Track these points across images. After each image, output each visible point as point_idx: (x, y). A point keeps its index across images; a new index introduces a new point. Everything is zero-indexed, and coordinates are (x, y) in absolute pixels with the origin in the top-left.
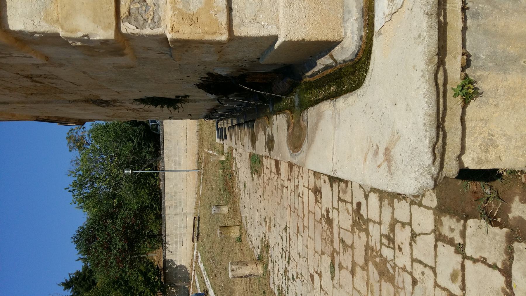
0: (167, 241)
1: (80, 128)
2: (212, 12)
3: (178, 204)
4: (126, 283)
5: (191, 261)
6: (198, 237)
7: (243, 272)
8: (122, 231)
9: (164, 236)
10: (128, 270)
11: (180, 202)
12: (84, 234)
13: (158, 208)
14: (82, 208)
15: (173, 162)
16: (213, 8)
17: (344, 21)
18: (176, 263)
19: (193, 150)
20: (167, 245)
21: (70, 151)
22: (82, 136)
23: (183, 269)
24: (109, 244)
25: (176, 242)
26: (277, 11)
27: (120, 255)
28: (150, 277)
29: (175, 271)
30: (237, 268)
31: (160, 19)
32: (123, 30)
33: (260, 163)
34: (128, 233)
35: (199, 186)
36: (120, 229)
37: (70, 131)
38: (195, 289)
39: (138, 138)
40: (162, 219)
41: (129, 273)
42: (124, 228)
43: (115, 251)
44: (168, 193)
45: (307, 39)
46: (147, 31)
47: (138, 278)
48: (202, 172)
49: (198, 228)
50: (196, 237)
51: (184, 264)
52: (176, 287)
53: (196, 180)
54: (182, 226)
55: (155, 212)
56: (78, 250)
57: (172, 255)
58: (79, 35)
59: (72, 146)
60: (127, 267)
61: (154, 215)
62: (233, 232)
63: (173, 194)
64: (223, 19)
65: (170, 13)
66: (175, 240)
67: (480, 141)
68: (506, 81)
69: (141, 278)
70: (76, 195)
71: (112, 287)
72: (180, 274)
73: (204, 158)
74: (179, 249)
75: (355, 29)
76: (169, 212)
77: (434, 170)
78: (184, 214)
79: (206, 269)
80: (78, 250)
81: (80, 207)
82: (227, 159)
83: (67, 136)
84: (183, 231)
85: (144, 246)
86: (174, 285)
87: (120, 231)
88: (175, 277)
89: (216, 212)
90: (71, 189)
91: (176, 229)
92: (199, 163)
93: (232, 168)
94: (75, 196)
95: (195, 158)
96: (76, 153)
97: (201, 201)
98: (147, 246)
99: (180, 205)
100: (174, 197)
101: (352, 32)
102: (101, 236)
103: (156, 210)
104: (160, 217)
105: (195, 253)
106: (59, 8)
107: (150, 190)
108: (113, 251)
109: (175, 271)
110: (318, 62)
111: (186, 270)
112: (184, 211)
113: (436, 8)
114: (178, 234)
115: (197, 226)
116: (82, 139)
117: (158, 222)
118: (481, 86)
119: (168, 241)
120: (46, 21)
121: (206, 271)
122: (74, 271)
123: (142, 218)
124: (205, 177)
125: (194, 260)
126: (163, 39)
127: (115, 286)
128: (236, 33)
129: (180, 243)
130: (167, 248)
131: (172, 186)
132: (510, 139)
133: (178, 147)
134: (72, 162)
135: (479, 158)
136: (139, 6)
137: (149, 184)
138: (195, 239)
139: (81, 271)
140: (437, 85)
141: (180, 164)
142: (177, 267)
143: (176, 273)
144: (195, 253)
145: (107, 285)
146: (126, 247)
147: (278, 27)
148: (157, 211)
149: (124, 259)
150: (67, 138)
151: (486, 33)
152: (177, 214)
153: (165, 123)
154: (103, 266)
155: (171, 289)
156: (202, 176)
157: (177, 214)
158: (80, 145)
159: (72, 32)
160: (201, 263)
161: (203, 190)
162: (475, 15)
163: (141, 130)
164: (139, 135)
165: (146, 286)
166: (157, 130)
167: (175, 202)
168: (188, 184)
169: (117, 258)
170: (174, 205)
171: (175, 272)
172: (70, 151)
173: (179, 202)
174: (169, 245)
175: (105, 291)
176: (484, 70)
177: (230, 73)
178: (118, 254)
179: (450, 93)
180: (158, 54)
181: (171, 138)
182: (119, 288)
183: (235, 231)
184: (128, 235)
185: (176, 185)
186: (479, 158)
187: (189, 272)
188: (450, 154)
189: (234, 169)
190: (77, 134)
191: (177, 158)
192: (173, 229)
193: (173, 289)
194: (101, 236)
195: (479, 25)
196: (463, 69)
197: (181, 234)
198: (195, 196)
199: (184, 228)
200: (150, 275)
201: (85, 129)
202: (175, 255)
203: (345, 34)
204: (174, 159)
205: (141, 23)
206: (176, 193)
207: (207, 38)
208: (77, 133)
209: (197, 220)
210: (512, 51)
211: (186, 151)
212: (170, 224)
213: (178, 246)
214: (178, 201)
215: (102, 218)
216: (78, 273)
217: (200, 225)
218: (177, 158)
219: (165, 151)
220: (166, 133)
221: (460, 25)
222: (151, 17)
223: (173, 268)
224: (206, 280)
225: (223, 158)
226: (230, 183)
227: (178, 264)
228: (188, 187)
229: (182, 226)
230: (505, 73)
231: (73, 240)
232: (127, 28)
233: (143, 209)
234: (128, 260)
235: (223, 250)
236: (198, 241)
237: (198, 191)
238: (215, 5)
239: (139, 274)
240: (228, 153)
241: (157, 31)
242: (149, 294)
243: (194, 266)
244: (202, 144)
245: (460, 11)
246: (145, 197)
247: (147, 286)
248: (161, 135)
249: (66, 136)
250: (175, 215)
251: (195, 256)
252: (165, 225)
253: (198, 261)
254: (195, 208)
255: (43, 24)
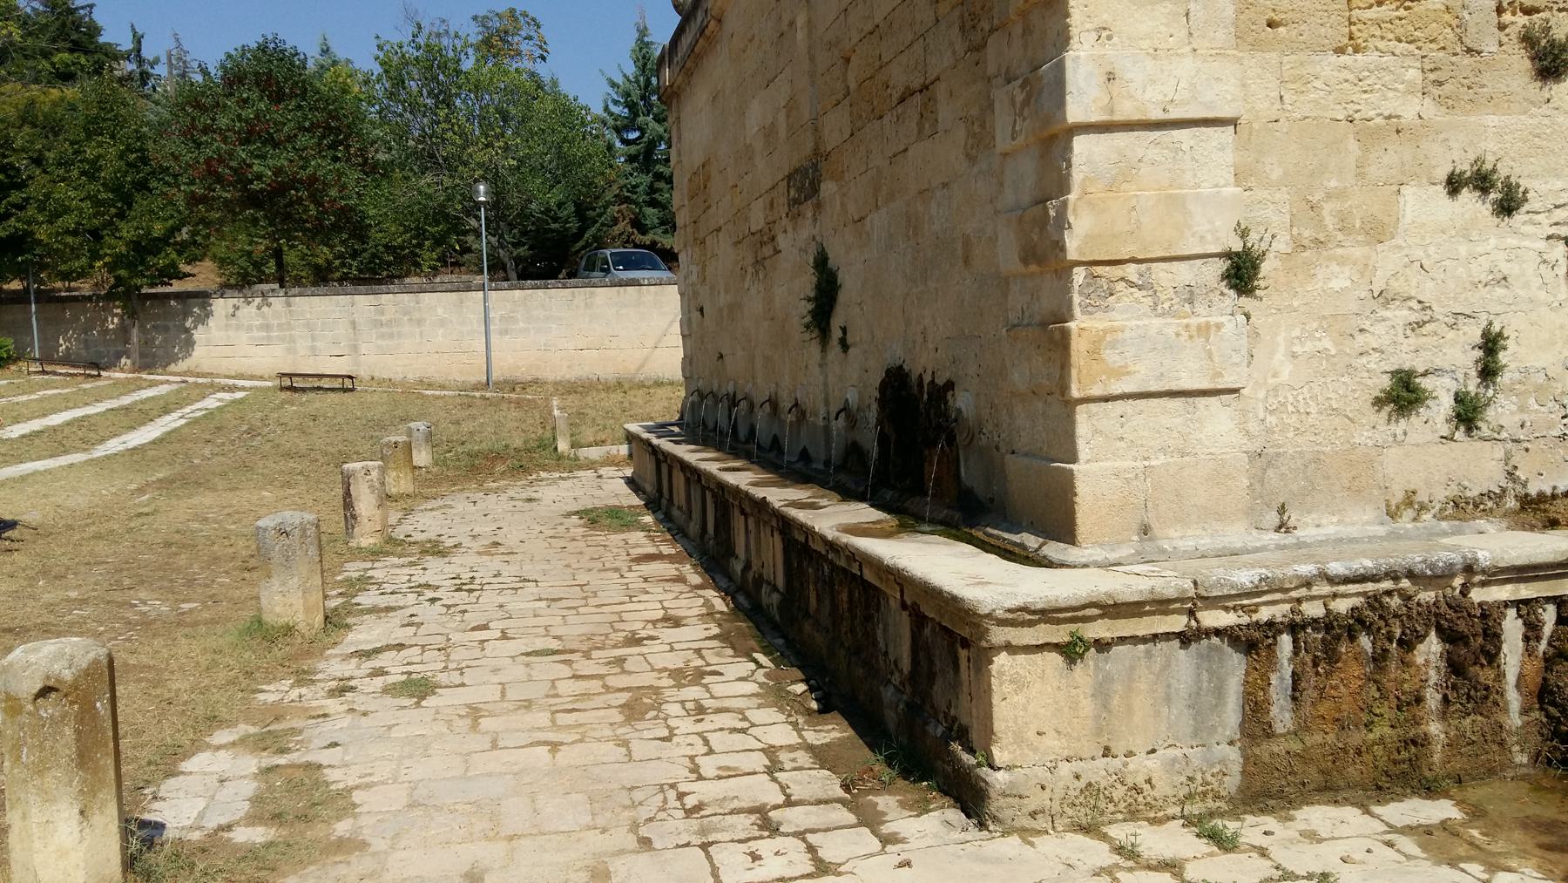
0: (271, 300)
1: (541, 47)
2: (1104, 377)
3: (384, 330)
4: (142, 186)
5: (209, 371)
6: (291, 389)
7: (362, 497)
8: (303, 175)
9: (286, 293)
10: (184, 191)
11: (391, 336)
12: (289, 69)
13: (348, 273)
14: (323, 51)
15: (512, 315)
16: (1109, 378)
17: (1101, 545)
18: (200, 327)
19: (546, 367)
20: (258, 300)
21: (475, 18)
22: (519, 53)
23: (180, 349)
24: (260, 137)
25: (267, 327)
26: (1107, 459)
27: (231, 168)
28: (163, 254)
29: (175, 326)
30: (372, 480)
31: (1091, 313)
32: (1076, 270)
33: (625, 528)
34: (297, 190)
35: (443, 387)
36: (310, 171)
37: (534, 20)
38: (133, 387)
39: (542, 213)
40: (315, 284)
41: (174, 194)
42: (313, 179)
43: (244, 156)
44: (417, 303)
45: (1077, 499)
46: (1077, 299)
47: (158, 219)
48: (488, 395)
49: (319, 388)
50: (291, 384)
51: (199, 352)
52: (124, 330)
53: (460, 378)
54: (318, 344)
55: (337, 262)
56: (236, 49)
57: (226, 316)
58: (1071, 219)
59: (490, 24)
60: (193, 188)
61: (327, 260)
62: (399, 477)
63: (417, 316)
64: (1097, 391)
65: (1100, 325)
66: (276, 322)
67: (1022, 672)
68: (1085, 698)
69: (158, 229)
70: (404, 50)
71: (129, 145)
72: (165, 340)
73: (530, 397)
74: (244, 336)
75: (1095, 558)
76: (362, 305)
77: (1000, 613)
78: (355, 348)
79: (211, 413)
80: (236, 49)
81: (325, 48)
82: (560, 458)
83: (518, 12)
84: (302, 346)
85: (257, 235)
86: (128, 322)
87: (304, 168)
88: (154, 326)
89: (415, 434)
90: (421, 40)
91: (309, 326)
92: (512, 385)
93: (544, 470)
94: (401, 47)
95: (523, 374)
96: (474, 34)
97: (402, 392)
98: (257, 243)
99: (382, 336)
100: (406, 318)
101: (1091, 555)
102: (285, 116)
103: (343, 265)
104: (322, 278)
105: (240, 383)
106: (1099, 195)
107: (403, 248)
108: (243, 150)
109: (175, 326)
110: (1024, 534)
111: (175, 359)
112: (363, 348)
113: (1158, 597)
114: (293, 332)
115: (326, 383)
116: (512, 53)
117: (303, 274)
118: (1079, 666)
119: (269, 305)
120: (1084, 179)
121: (204, 416)
122: (99, 17)
123: (336, 228)
124: (478, 402)
125: (217, 380)
126: (1065, 315)
127: (132, 153)
128: (1079, 408)
129: (263, 338)
130: (249, 303)
131: (440, 311)
132: (1025, 709)
133: (554, 326)
134: (444, 21)
135: (1003, 674)
136: (1105, 288)
137: (420, 246)
138: (286, 382)
139: (101, 40)
140: (1084, 607)
141: (505, 332)
142: (187, 331)
143: (167, 329)
144: (240, 383)
145: (136, 131)
146: (256, 186)
147: (1088, 461)
148: (337, 269)
149: (219, 179)
150: (512, 11)
151: (1132, 668)
152: (354, 328)
153: (618, 292)
154: (193, 119)
155: (116, 315)
156: (477, 394)
157: (354, 328)
158: (492, 46)
159: (1074, 210)
160: (220, 400)
161: (438, 398)
162: (1149, 655)
163: (567, 222)
164: (551, 218)
165: (131, 242)
166: (591, 267)
167: (390, 321)
168: (445, 355)
169: (221, 161)
170: (383, 318)
171: (171, 327)
172: (475, 18)
173: (392, 333)
174: (259, 308)
175: (117, 125)
176: (1095, 669)
177: (966, 416)
178: (233, 164)
179: (1073, 627)
180: (1020, 307)
181: (577, 307)
182: (129, 164)
183: (402, 482)
184: (293, 192)
185: (442, 323)
186: (1003, 674)
187: (172, 367)
188: (1012, 633)
189: (543, 474)
190: (525, 39)
191: (521, 325)
192: (308, 316)
193: (116, 320)
194: (285, 116)
195: (1139, 658)
196: (1097, 641)
197: (292, 340)
198: (411, 377)
199: (313, 348)
200: (167, 255)
201: (539, 60)
202: (226, 325)
203: (1086, 548)
204: (519, 317)
205: (1086, 291)
206: (420, 322)
207: (1074, 372)
208: (529, 38)
209: (346, 384)
210: (1116, 701)
211: (543, 348)
212: (323, 308)
213: (256, 334)
214: (395, 330)
215: (333, 118)
216: (94, 30)
217: (332, 395)
218: (521, 325)
219: (540, 292)
220: (592, 293)
221: (1140, 633)
222: (1092, 302)
223: (185, 319)
224: (175, 415)
225: (563, 446)
226: (500, 468)
227: (199, 335)
228: (437, 356)
229: (318, 344)
230: (1093, 695)
231: (270, 37)
232: (1079, 275)
233: (359, 231)
234: (214, 191)
235: (298, 459)
236: (282, 389)
237: (430, 386)
238: (1112, 380)
239: (171, 222)
240: (577, 458)
241: (1077, 311)
242: (109, 252)
243: (200, 380)
244: (569, 393)
245: (1153, 632)
246: (381, 235)
247: (136, 245)
248: (587, 281)
249: (520, 9)
250: (353, 323)
251: (231, 382)
252: (320, 293)
253: (218, 391)
254: (373, 378)
255: (1081, 176)
